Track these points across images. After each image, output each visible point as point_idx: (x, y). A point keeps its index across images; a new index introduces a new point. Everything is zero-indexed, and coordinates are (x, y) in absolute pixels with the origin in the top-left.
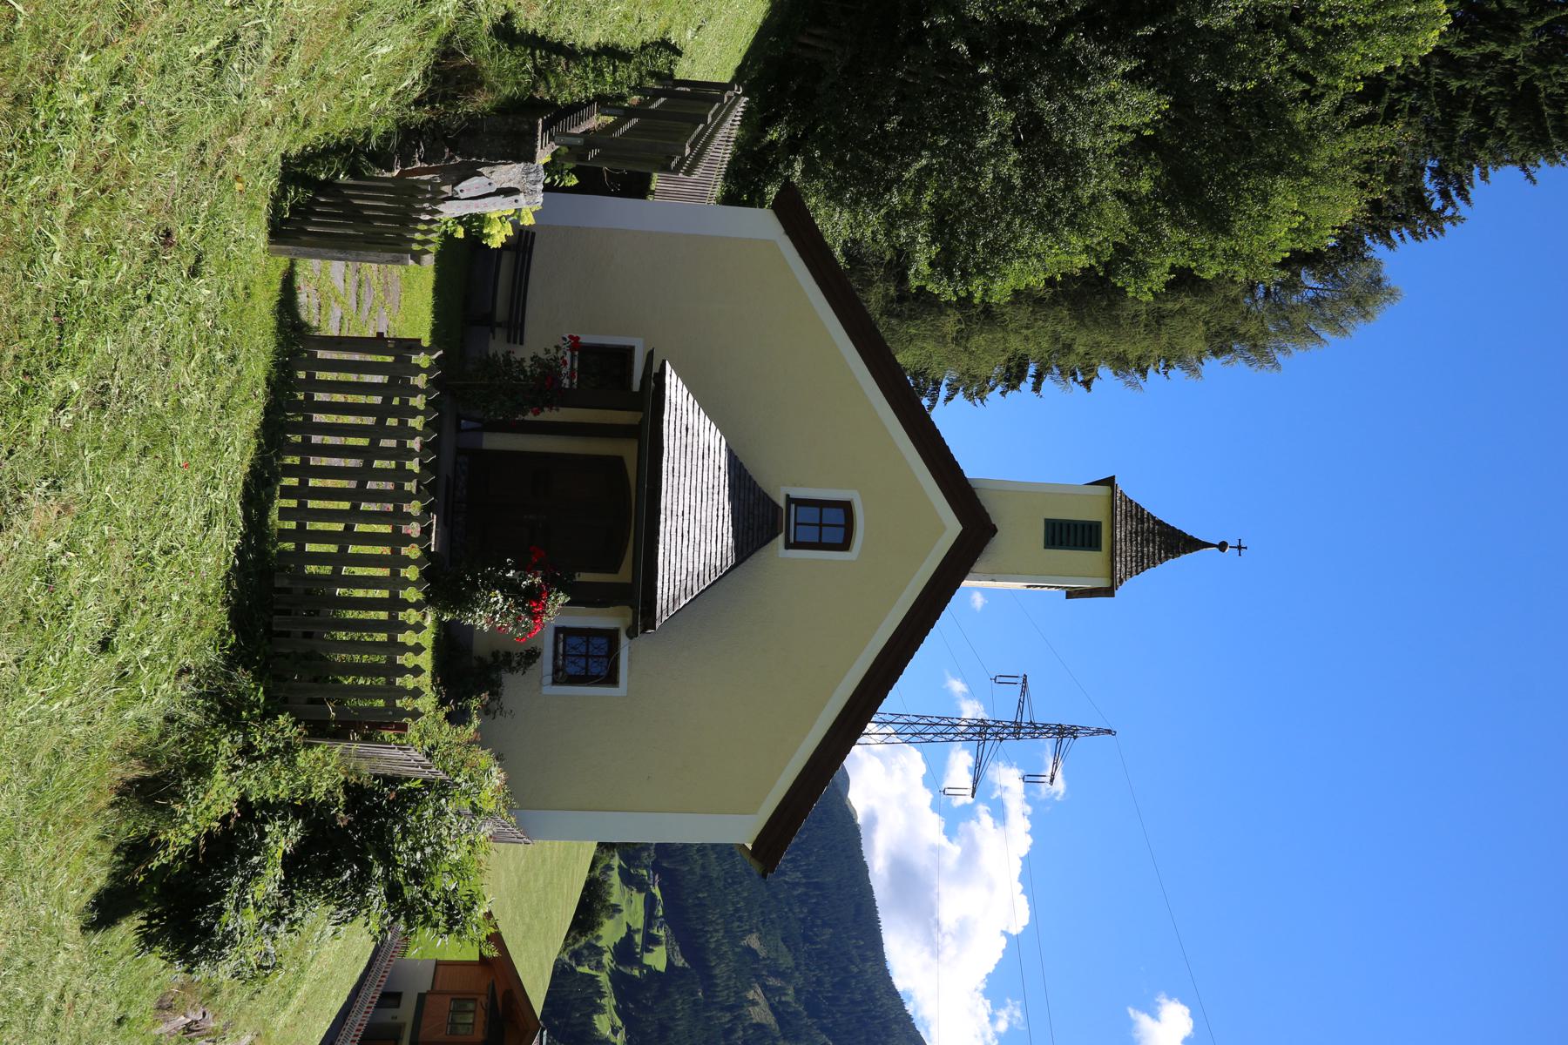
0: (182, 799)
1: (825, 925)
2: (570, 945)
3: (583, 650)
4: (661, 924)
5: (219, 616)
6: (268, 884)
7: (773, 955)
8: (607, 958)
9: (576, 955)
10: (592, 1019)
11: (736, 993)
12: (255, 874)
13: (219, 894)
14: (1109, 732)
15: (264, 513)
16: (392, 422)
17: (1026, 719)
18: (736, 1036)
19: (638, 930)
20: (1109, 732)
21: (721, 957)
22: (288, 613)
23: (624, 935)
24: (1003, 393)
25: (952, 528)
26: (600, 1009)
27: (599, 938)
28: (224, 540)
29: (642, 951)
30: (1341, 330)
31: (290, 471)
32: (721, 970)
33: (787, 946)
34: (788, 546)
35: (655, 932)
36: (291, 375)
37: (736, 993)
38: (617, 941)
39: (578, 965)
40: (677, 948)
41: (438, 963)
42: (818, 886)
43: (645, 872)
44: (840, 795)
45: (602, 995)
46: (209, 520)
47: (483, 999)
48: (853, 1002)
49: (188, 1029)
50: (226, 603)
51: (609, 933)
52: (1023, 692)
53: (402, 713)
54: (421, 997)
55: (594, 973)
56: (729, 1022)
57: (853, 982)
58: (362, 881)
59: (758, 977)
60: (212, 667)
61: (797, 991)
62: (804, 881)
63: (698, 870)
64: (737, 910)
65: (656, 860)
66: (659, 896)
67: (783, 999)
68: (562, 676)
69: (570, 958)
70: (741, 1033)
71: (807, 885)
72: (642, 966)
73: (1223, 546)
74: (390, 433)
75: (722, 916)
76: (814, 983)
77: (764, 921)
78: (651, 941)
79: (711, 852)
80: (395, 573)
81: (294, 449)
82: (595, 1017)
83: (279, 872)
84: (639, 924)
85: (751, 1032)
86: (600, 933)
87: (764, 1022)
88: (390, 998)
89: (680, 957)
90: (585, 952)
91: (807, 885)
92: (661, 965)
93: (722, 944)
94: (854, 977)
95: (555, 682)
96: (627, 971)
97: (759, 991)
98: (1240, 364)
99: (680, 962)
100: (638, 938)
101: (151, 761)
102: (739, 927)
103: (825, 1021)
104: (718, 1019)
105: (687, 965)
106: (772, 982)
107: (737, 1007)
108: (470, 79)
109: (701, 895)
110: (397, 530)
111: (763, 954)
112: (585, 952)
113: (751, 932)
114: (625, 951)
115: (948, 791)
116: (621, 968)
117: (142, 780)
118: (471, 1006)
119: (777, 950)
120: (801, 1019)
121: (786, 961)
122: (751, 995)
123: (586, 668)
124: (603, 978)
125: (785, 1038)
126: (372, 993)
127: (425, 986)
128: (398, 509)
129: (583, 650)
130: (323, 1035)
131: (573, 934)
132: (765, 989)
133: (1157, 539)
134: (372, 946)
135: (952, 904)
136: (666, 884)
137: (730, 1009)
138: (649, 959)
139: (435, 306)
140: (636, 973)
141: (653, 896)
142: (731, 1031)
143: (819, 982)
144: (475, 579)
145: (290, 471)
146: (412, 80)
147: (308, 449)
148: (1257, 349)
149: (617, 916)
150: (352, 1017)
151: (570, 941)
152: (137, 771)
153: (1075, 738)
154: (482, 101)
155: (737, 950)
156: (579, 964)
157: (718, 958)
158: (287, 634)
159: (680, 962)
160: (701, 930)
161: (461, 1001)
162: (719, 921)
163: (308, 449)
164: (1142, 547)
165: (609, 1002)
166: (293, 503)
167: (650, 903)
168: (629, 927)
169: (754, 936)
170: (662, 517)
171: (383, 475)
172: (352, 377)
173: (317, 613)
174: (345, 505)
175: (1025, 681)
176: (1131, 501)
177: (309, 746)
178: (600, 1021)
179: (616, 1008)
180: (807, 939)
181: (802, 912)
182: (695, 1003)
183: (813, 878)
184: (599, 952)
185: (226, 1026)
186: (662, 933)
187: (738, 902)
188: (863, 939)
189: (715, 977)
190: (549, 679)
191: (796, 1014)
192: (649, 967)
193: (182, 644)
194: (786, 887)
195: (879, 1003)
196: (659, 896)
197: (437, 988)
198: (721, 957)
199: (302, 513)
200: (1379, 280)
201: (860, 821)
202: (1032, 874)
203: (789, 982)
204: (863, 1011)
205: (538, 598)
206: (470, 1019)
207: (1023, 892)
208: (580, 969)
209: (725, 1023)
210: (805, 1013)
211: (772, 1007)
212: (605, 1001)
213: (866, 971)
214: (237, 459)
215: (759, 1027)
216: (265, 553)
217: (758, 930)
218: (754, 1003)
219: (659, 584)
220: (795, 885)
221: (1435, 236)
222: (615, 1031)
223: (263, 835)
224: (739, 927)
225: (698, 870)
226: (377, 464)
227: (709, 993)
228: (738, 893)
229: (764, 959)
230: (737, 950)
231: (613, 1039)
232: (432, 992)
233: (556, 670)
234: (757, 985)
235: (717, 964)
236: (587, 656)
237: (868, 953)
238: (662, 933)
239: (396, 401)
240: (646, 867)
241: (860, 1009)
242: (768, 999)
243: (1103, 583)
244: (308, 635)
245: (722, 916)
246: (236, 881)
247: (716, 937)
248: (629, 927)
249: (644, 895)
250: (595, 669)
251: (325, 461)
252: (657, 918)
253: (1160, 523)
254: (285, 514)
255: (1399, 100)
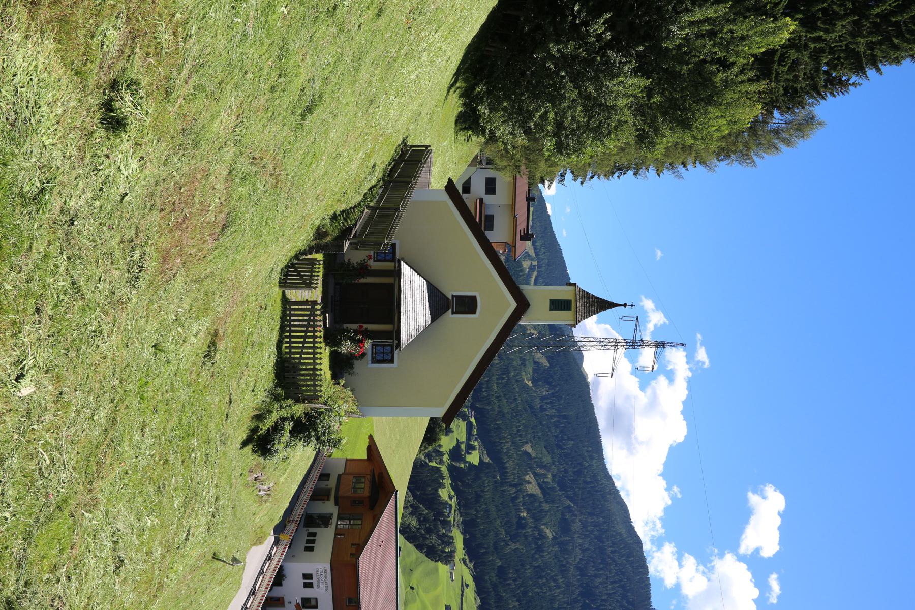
0: (266, 419)
1: (569, 439)
2: (423, 451)
3: (382, 351)
4: (476, 438)
5: (273, 376)
6: (286, 436)
7: (540, 456)
8: (446, 458)
9: (428, 456)
10: (438, 491)
11: (519, 477)
12: (282, 435)
13: (274, 440)
14: (682, 344)
15: (281, 348)
16: (311, 323)
17: (638, 338)
18: (519, 500)
19: (463, 442)
20: (682, 344)
21: (510, 457)
22: (288, 372)
23: (455, 445)
24: (618, 177)
25: (513, 305)
26: (442, 486)
27: (440, 446)
28: (273, 359)
29: (465, 454)
30: (788, 142)
31: (286, 337)
32: (510, 464)
33: (548, 451)
34: (453, 313)
35: (472, 443)
36: (286, 313)
37: (519, 477)
38: (451, 448)
39: (430, 461)
40: (485, 452)
41: (347, 460)
42: (565, 417)
43: (466, 410)
44: (577, 365)
45: (443, 478)
46: (270, 356)
47: (368, 477)
48: (585, 482)
49: (256, 479)
50: (274, 373)
51: (446, 443)
52: (636, 325)
53: (318, 396)
54: (339, 476)
55: (438, 466)
56: (515, 493)
57: (585, 471)
58: (309, 436)
59: (531, 468)
60: (272, 388)
61: (554, 476)
62: (557, 414)
63: (496, 409)
64: (518, 431)
65: (472, 403)
66: (474, 423)
67: (545, 480)
68: (375, 361)
69: (425, 458)
70: (522, 499)
71: (559, 416)
72: (465, 462)
73: (625, 305)
74: (311, 326)
75: (510, 434)
76: (563, 471)
77: (534, 437)
78: (470, 448)
79: (503, 398)
80: (314, 362)
81: (287, 332)
82: (440, 490)
83: (288, 434)
84: (463, 438)
85: (527, 498)
86: (442, 444)
87: (535, 493)
88: (324, 476)
89: (487, 457)
90: (434, 454)
91: (559, 416)
92: (476, 462)
93: (510, 450)
94: (585, 468)
95: (372, 363)
96: (457, 464)
97: (532, 476)
98: (736, 164)
99: (487, 459)
100: (463, 447)
101: (259, 410)
102: (520, 440)
103: (569, 493)
104: (508, 491)
105: (490, 461)
106: (539, 471)
107: (519, 485)
108: (326, 234)
109: (498, 423)
110: (314, 334)
111: (534, 455)
112: (434, 454)
113: (527, 443)
114: (456, 454)
115: (598, 375)
116: (454, 463)
117: (257, 415)
118: (363, 480)
119: (542, 454)
120: (555, 492)
121: (547, 459)
122: (527, 478)
123: (383, 357)
124: (444, 469)
125: (547, 502)
126: (316, 474)
127: (341, 471)
128: (314, 334)
129: (382, 351)
130: (295, 491)
131: (424, 444)
132: (535, 474)
133: (596, 305)
134: (315, 453)
135: (643, 426)
136: (478, 416)
137: (515, 486)
138: (469, 458)
139: (323, 291)
140: (462, 466)
141: (471, 423)
142: (516, 498)
143: (566, 471)
144: (341, 338)
145: (286, 337)
146: (311, 236)
147: (291, 331)
148: (745, 157)
149: (451, 434)
150: (307, 485)
151: (423, 448)
152: (256, 413)
153: (664, 347)
154: (329, 239)
155: (520, 453)
156: (430, 461)
157: (508, 458)
158: (288, 378)
159: (487, 459)
160: (499, 442)
161: (358, 477)
162: (508, 437)
163: (291, 331)
164: (589, 307)
165: (447, 482)
166: (288, 345)
167: (469, 427)
168: (458, 440)
169: (529, 445)
170: (402, 314)
171: (310, 337)
172: (301, 323)
173: (295, 372)
174: (302, 340)
175: (637, 319)
176: (584, 291)
177: (295, 405)
178: (443, 493)
179: (451, 485)
180: (559, 447)
181: (556, 432)
182: (496, 482)
183: (562, 412)
184: (441, 454)
185: (266, 479)
186: (476, 444)
187: (519, 426)
188: (591, 447)
189: (506, 468)
190: (370, 362)
191: (553, 489)
192: (469, 463)
193: (266, 385)
194: (547, 418)
195: (600, 483)
196: (474, 423)
197: (347, 472)
198: (510, 457)
199: (290, 348)
200: (813, 117)
201: (590, 378)
202: (690, 410)
203: (548, 471)
204: (591, 487)
205: (362, 342)
206: (363, 486)
207: (684, 420)
208: (431, 464)
209: (513, 494)
210: (558, 488)
211: (539, 485)
212: (445, 481)
213: (592, 465)
214: (275, 337)
215: (532, 495)
216: (282, 357)
217: (531, 442)
218: (529, 482)
219: (401, 336)
220: (551, 417)
221: (843, 94)
222: (451, 498)
223: (284, 425)
224: (520, 440)
225: (496, 409)
226: (308, 334)
227: (503, 477)
228: (519, 421)
229: (534, 458)
230: (520, 453)
231: (449, 502)
232: (344, 473)
233: (373, 358)
234: (530, 472)
235: (508, 461)
236: (383, 353)
237: (594, 455)
238: (476, 444)
239: (312, 318)
240: (467, 407)
241: (589, 486)
242: (537, 480)
243: (572, 322)
244: (294, 378)
245: (510, 434)
246: (278, 437)
247: (507, 446)
248: (458, 440)
249: (466, 422)
250: (386, 357)
251: (295, 334)
252: (473, 435)
253: (598, 298)
254: (286, 348)
255: (787, 52)
